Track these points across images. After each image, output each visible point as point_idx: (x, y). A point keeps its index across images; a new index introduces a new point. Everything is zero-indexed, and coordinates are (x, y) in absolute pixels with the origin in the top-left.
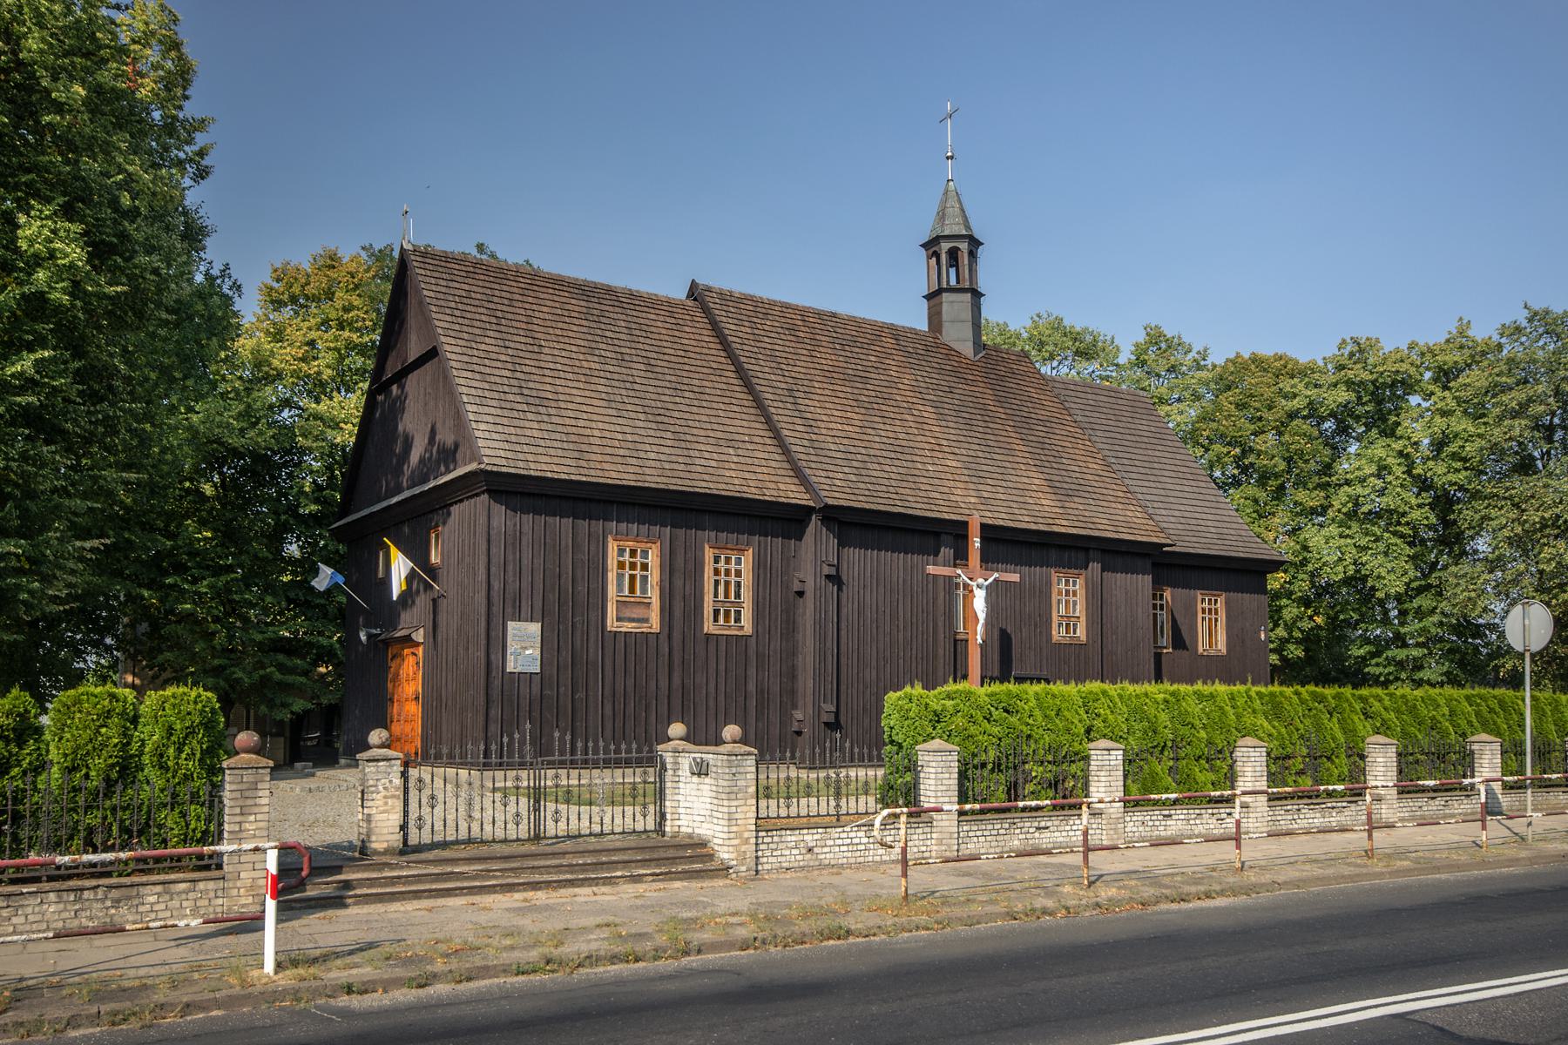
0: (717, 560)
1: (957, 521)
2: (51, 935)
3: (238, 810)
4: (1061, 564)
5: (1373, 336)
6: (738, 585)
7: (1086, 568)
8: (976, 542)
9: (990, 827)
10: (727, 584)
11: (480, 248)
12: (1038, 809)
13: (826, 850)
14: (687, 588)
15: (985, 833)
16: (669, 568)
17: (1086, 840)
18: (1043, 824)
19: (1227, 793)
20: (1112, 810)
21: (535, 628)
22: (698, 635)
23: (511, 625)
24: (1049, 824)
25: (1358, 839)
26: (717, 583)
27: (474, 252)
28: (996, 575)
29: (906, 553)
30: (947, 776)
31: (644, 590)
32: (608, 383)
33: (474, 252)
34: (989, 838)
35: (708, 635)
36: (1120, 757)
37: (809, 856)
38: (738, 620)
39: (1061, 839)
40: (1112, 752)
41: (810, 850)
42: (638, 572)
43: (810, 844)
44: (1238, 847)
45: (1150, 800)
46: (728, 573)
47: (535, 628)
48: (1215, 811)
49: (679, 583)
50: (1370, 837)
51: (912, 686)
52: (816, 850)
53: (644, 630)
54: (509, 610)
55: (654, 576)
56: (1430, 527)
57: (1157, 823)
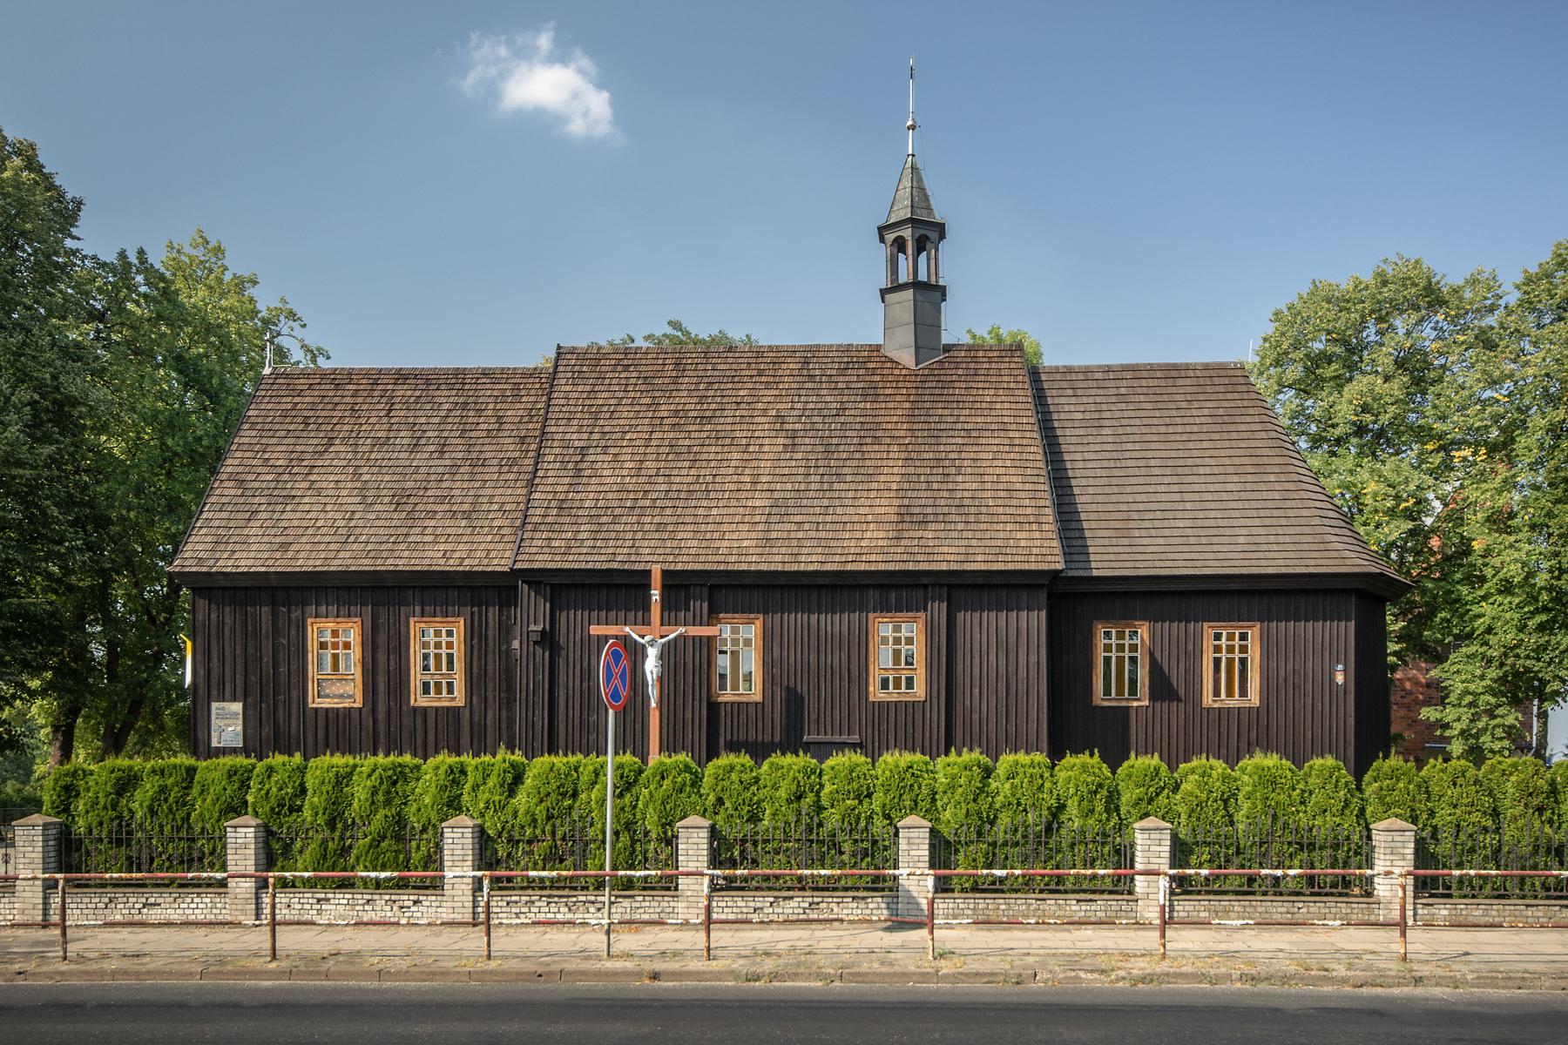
0: (1218, 637)
1: (701, 571)
3: (1389, 851)
4: (885, 608)
5: (31, 139)
6: (1243, 662)
7: (687, 609)
8: (656, 595)
9: (87, 900)
10: (1230, 662)
11: (675, 325)
14: (392, 663)
16: (371, 645)
18: (152, 900)
19: (219, 875)
20: (238, 890)
21: (237, 707)
22: (404, 708)
23: (214, 705)
24: (159, 901)
25: (260, 939)
26: (1217, 662)
27: (670, 331)
28: (682, 630)
30: (30, 849)
31: (347, 667)
33: (670, 331)
34: (85, 911)
35: (415, 709)
36: (252, 835)
38: (450, 691)
40: (239, 830)
46: (438, 645)
47: (237, 707)
48: (397, 897)
49: (382, 658)
51: (1092, 755)
53: (347, 705)
54: (214, 692)
55: (356, 654)
57: (308, 907)
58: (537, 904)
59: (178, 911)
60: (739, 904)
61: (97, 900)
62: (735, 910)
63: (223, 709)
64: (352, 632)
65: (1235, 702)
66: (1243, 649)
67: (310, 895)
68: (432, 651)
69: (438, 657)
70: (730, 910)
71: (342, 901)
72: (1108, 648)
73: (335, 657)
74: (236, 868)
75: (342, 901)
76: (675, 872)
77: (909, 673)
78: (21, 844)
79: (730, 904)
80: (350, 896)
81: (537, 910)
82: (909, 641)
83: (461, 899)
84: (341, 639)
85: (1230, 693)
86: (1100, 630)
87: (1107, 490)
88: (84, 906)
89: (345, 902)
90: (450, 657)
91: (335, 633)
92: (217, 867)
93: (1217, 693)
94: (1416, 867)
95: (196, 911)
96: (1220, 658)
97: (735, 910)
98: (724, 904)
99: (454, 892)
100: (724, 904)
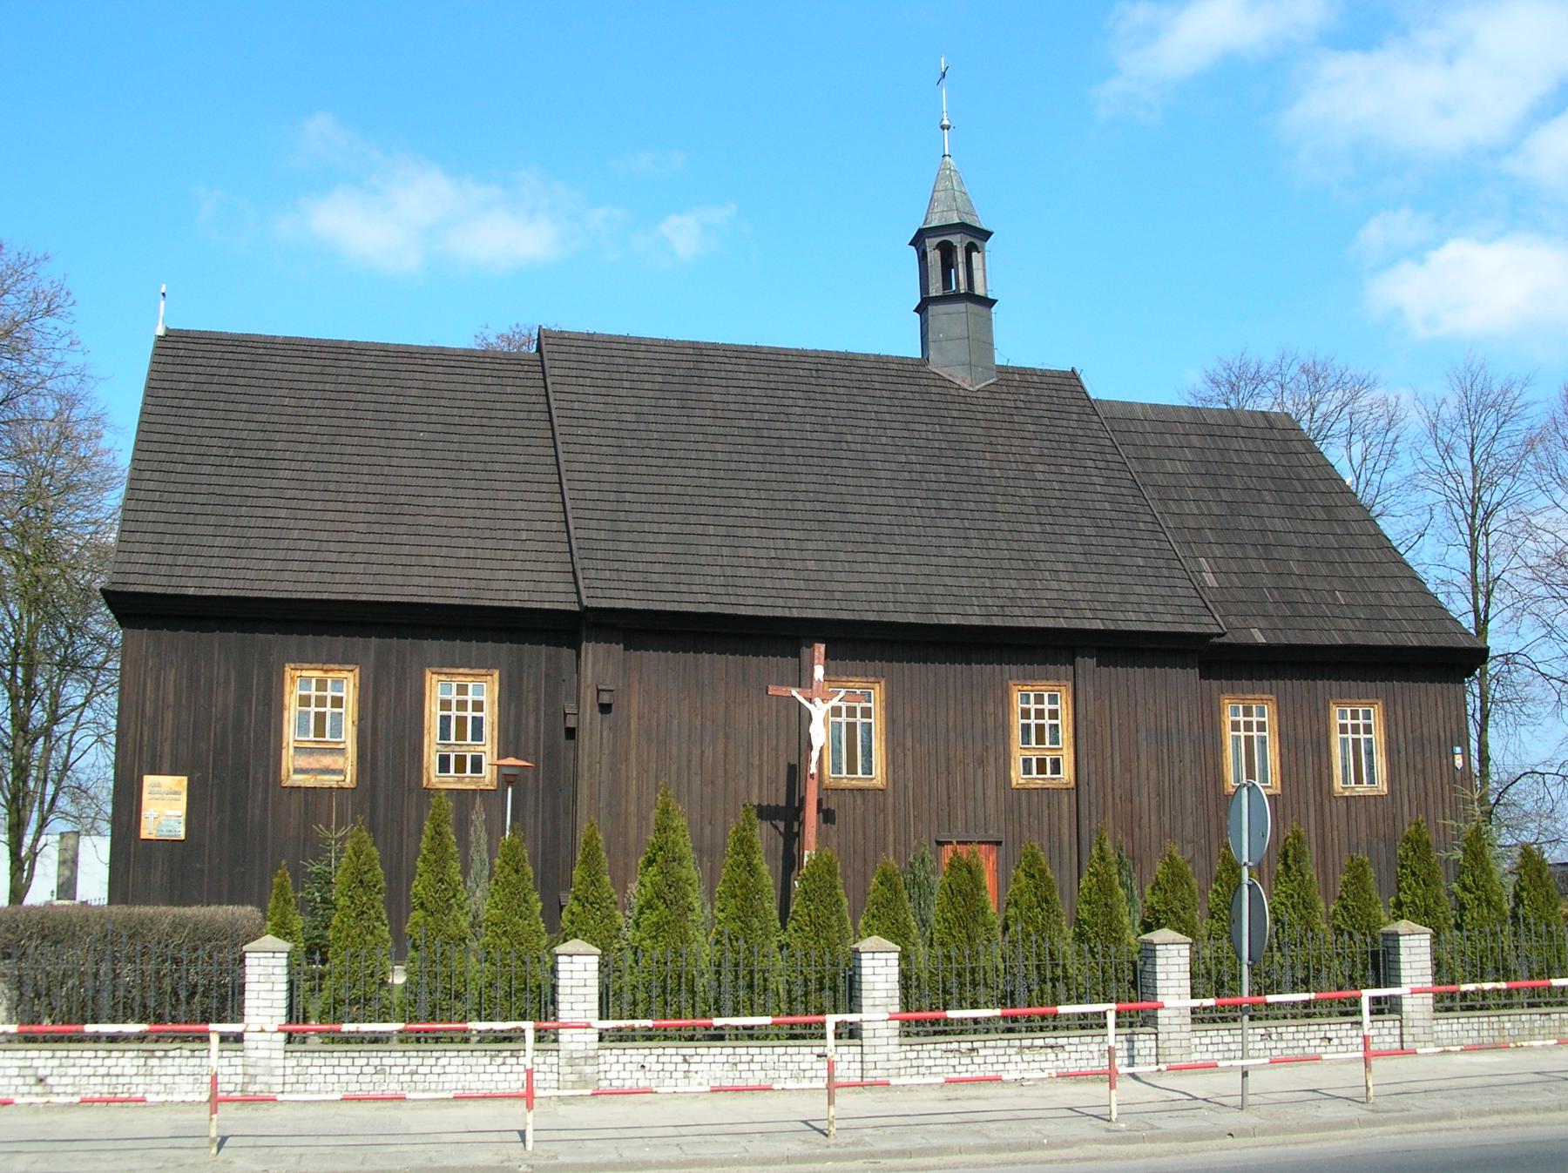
2: (589, 1092)
12: (376, 1039)
13: (65, 1080)
15: (338, 1070)
17: (831, 1076)
21: (179, 783)
23: (149, 780)
29: (925, 662)
32: (601, 424)
37: (39, 1089)
39: (480, 1085)
41: (41, 1080)
42: (328, 709)
43: (41, 1072)
44: (530, 1106)
45: (947, 1022)
47: (179, 783)
50: (831, 1102)
52: (49, 1081)
55: (349, 712)
56: (101, 553)
57: (672, 1067)
58: (982, 1052)
59: (483, 1077)
60: (1226, 1039)
61: (364, 1061)
62: (1221, 1047)
63: (159, 785)
64: (347, 685)
65: (1363, 789)
66: (1368, 729)
67: (673, 1051)
68: (454, 713)
69: (461, 721)
70: (1214, 1048)
71: (718, 1059)
72: (1026, 714)
73: (320, 717)
74: (573, 1014)
75: (718, 1059)
76: (555, 1024)
77: (1054, 755)
78: (255, 978)
79: (1215, 1040)
80: (730, 1051)
81: (981, 1060)
82: (1261, 727)
83: (885, 1049)
84: (470, 698)
85: (1358, 780)
86: (1335, 711)
87: (524, 486)
88: (342, 1070)
89: (724, 1059)
90: (478, 722)
91: (321, 684)
92: (728, 1011)
93: (1345, 781)
94: (289, 1022)
95: (510, 1077)
96: (1028, 726)
97: (1221, 1047)
98: (1207, 1041)
99: (876, 1042)
100: (1207, 1041)
